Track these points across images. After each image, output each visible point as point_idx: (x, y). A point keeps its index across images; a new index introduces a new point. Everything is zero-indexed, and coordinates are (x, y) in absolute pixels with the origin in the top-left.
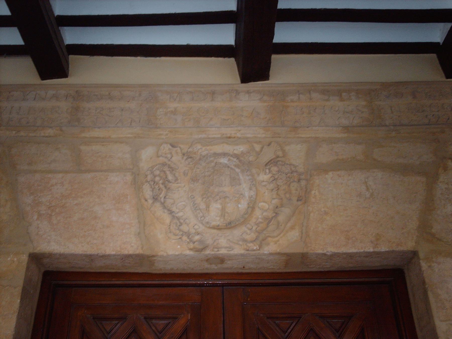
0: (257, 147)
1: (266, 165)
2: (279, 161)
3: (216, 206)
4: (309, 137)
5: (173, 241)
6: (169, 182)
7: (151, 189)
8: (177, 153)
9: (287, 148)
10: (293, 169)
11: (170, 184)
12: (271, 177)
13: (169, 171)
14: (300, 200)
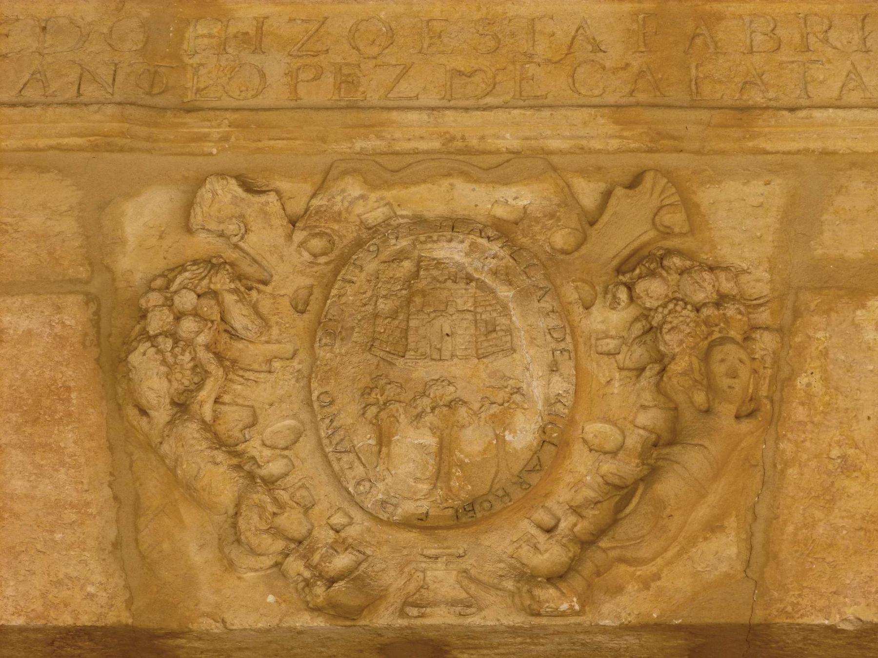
0: (588, 193)
1: (619, 271)
2: (669, 252)
3: (414, 442)
4: (798, 152)
5: (250, 574)
6: (234, 335)
7: (163, 369)
8: (265, 214)
9: (705, 196)
10: (727, 286)
11: (239, 345)
12: (637, 319)
13: (236, 291)
14: (750, 415)
